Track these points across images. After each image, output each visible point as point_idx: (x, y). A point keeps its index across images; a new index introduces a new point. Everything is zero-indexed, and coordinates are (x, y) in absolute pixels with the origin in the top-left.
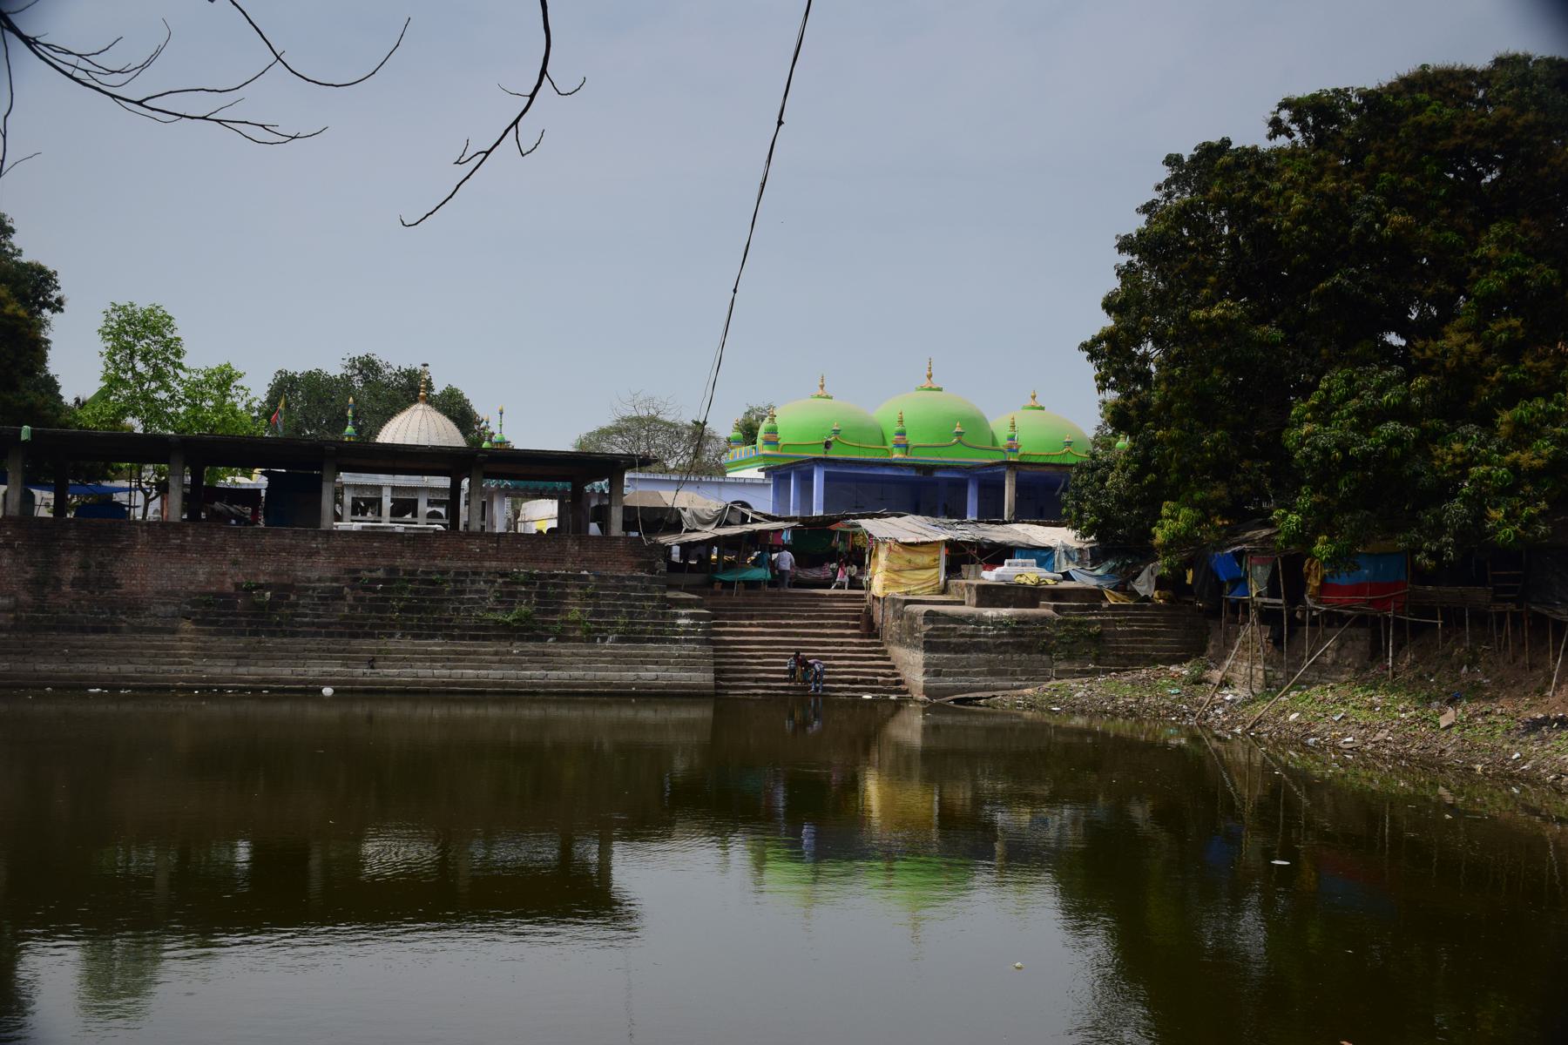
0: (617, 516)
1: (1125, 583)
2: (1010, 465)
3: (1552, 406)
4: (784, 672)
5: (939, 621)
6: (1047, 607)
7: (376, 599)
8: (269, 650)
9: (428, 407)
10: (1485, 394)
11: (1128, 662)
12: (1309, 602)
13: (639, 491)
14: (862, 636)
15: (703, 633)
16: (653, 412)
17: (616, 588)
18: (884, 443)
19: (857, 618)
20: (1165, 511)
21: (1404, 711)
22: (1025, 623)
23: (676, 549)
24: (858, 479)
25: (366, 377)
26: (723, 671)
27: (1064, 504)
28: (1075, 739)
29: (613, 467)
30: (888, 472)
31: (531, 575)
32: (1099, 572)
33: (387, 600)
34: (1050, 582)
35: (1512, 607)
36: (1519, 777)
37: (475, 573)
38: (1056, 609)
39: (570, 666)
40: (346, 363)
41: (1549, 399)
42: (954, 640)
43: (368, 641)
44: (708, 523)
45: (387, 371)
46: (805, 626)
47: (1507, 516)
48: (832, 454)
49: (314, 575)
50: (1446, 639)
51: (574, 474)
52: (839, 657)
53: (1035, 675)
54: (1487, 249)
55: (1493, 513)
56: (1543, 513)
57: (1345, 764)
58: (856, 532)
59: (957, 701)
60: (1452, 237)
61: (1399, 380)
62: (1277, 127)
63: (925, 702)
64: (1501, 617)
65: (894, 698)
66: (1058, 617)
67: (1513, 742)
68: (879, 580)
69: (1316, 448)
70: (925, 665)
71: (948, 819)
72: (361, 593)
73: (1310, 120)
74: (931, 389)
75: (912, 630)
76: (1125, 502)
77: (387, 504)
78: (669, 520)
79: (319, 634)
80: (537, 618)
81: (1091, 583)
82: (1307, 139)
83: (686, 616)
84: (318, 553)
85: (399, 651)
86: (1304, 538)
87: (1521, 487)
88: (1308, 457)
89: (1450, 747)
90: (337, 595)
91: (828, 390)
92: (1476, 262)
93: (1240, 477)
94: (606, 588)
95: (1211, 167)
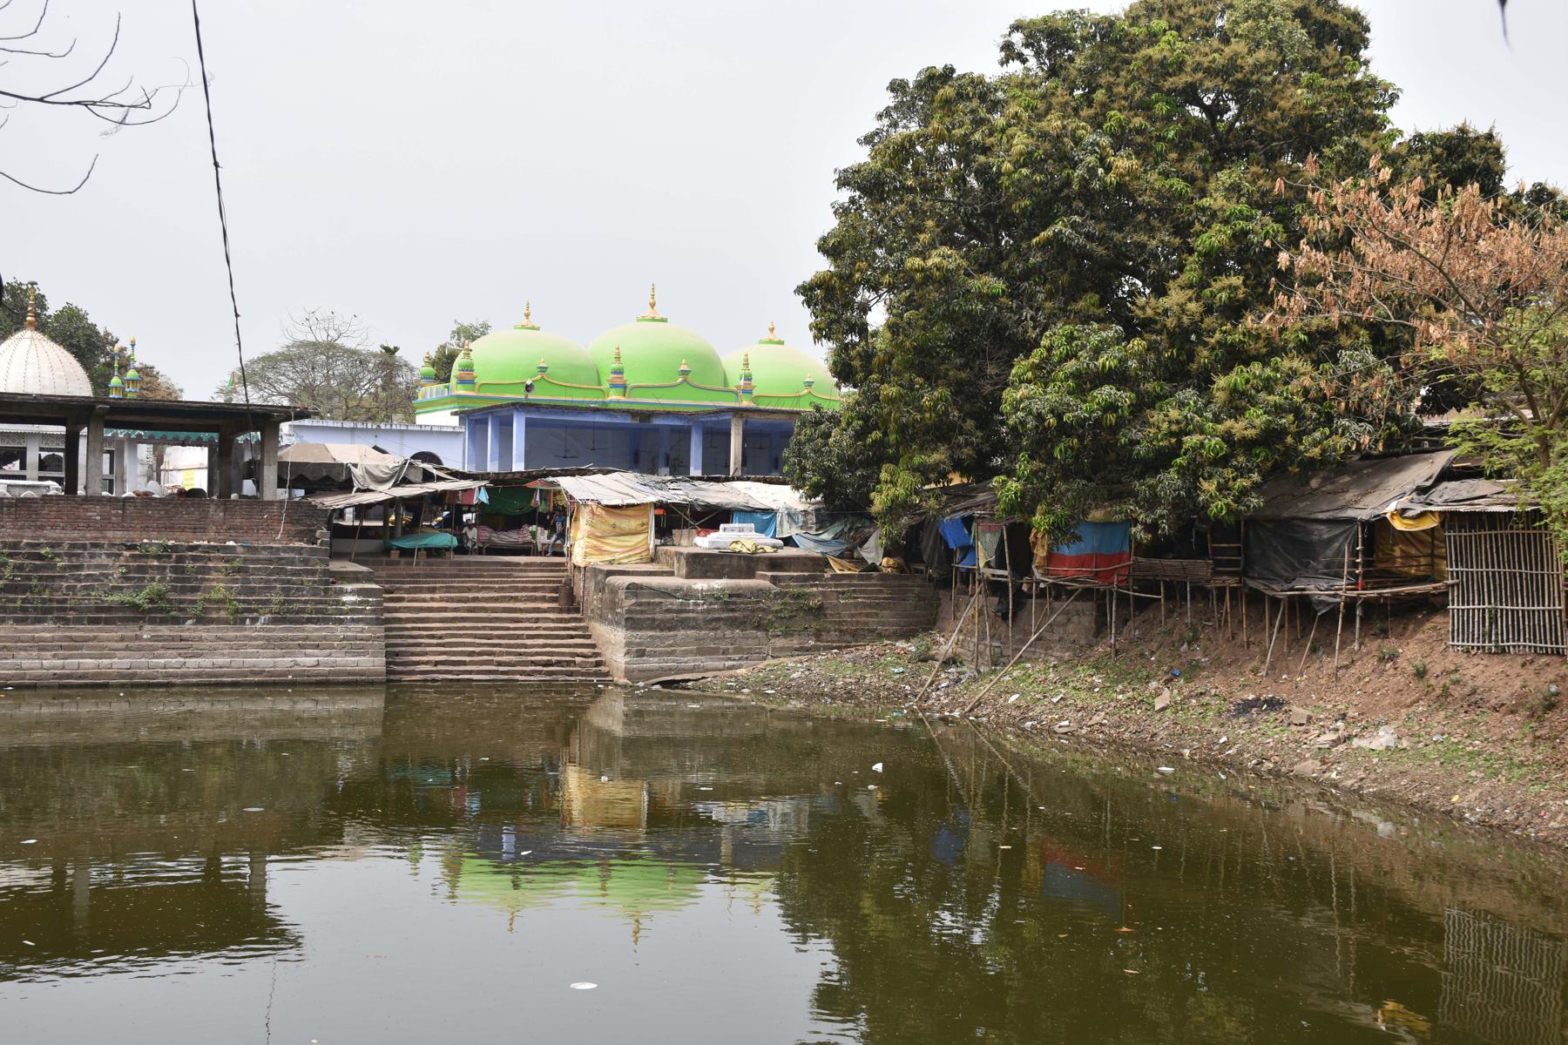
0: (270, 474)
1: (851, 550)
3: (1268, 371)
5: (643, 596)
6: (764, 577)
9: (38, 335)
10: (1204, 355)
11: (853, 636)
13: (295, 443)
14: (560, 611)
15: (373, 612)
16: (333, 334)
17: (270, 561)
19: (555, 590)
20: (884, 476)
21: (1122, 692)
22: (738, 596)
26: (397, 654)
28: (793, 725)
29: (266, 420)
30: (599, 419)
31: (166, 548)
32: (825, 536)
34: (769, 549)
35: (1232, 582)
36: (1224, 763)
37: (95, 545)
38: (774, 580)
42: (659, 616)
46: (496, 600)
47: (1220, 488)
48: (533, 397)
50: (1170, 613)
53: (747, 654)
55: (1205, 485)
56: (1256, 486)
57: (1062, 749)
58: (554, 493)
59: (664, 684)
60: (1179, 184)
61: (1118, 341)
63: (625, 686)
64: (1221, 591)
65: (595, 681)
67: (1222, 725)
68: (582, 546)
69: (1030, 413)
70: (628, 644)
71: (659, 817)
73: (1044, 45)
74: (653, 319)
75: (613, 605)
76: (849, 463)
78: (336, 479)
80: (172, 596)
83: (353, 592)
86: (1024, 504)
87: (1234, 456)
88: (1023, 423)
89: (1161, 729)
93: (961, 439)
94: (257, 561)
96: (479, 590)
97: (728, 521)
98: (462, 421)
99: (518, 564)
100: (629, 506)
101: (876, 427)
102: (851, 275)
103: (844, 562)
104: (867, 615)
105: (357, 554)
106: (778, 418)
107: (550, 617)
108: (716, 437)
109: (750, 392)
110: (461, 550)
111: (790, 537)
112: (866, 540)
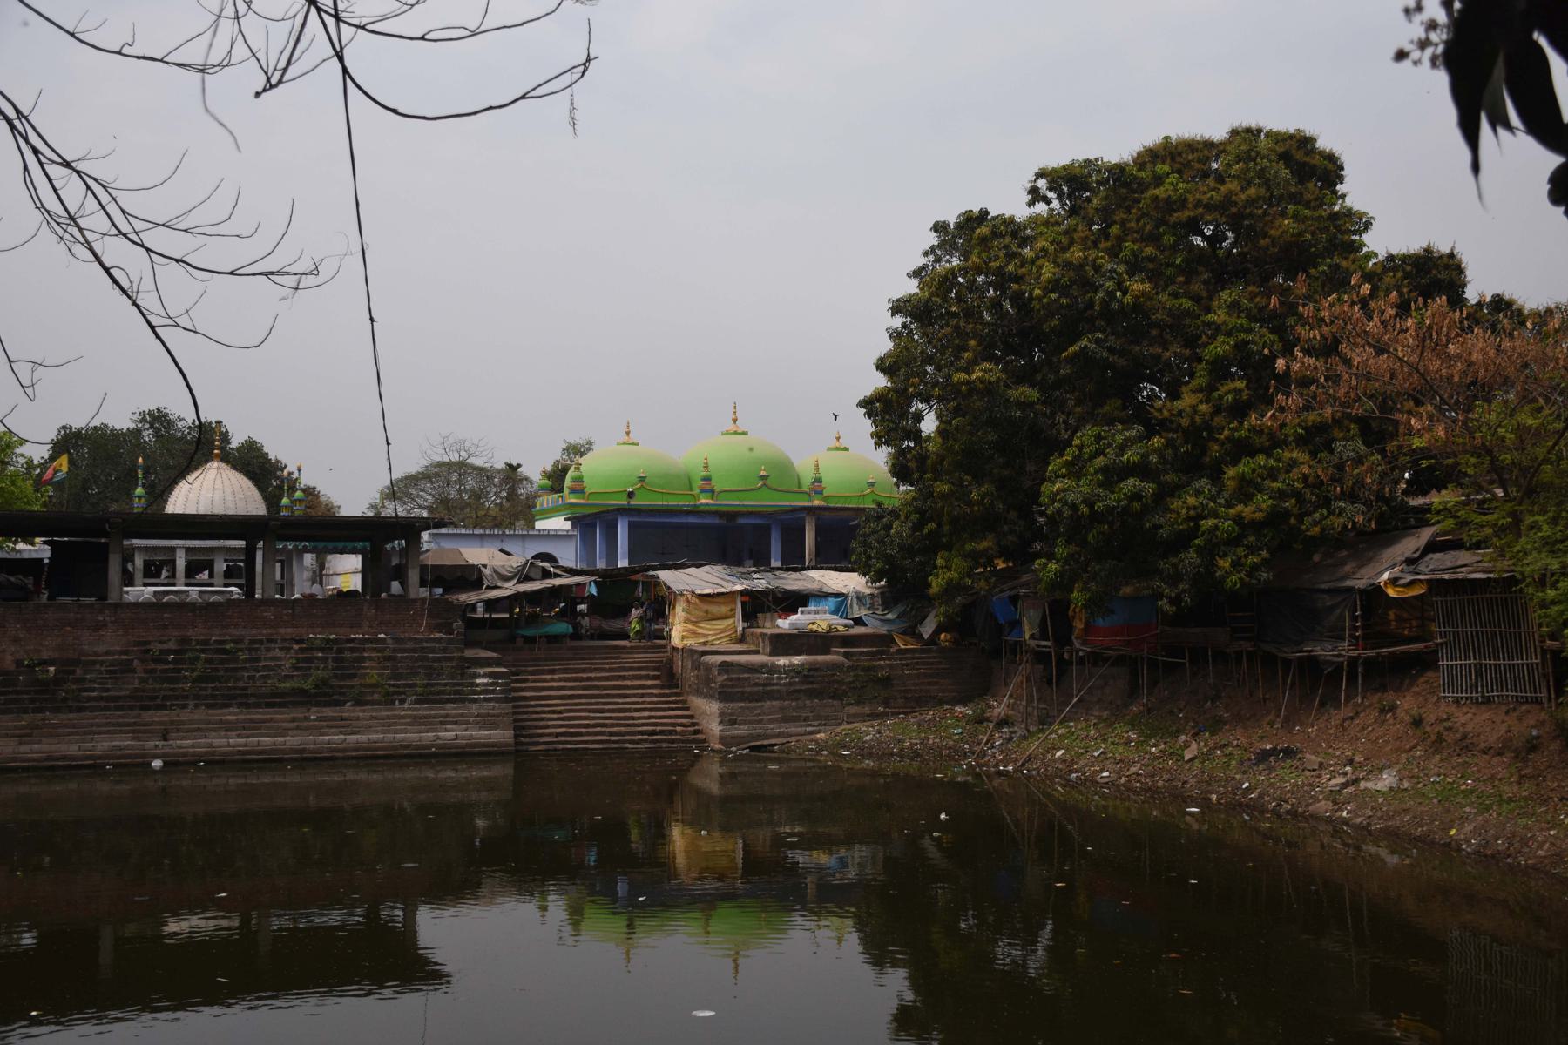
0: (413, 576)
1: (914, 627)
2: (811, 510)
3: (1272, 462)
6: (837, 653)
7: (166, 671)
8: (54, 726)
9: (223, 465)
11: (915, 702)
12: (1077, 645)
14: (662, 687)
15: (502, 692)
16: (464, 454)
17: (414, 650)
20: (940, 562)
23: (480, 607)
25: (157, 431)
26: (524, 728)
27: (853, 551)
29: (409, 529)
30: (691, 520)
32: (889, 616)
33: (179, 671)
34: (841, 629)
36: (1247, 805)
37: (269, 641)
38: (846, 655)
39: (368, 729)
40: (136, 417)
41: (1269, 456)
43: (159, 713)
44: (507, 579)
45: (180, 425)
46: (607, 679)
49: (102, 648)
51: (374, 536)
53: (826, 721)
54: (1219, 316)
55: (1221, 563)
56: (1265, 562)
58: (657, 583)
59: (752, 749)
60: (1187, 303)
61: (1140, 439)
62: (1035, 195)
65: (691, 746)
66: (848, 663)
68: (679, 631)
69: (1066, 503)
70: (721, 715)
71: (754, 865)
72: (153, 666)
74: (736, 433)
75: (708, 681)
76: (907, 550)
77: (181, 563)
78: (470, 577)
79: (106, 708)
80: (334, 682)
82: (1062, 205)
83: (485, 676)
84: (105, 626)
85: (191, 722)
86: (1063, 584)
88: (1059, 512)
90: (127, 668)
91: (634, 437)
92: (1209, 324)
93: (1006, 528)
95: (971, 233)
96: (592, 670)
98: (574, 526)
100: (719, 594)
101: (931, 519)
102: (906, 389)
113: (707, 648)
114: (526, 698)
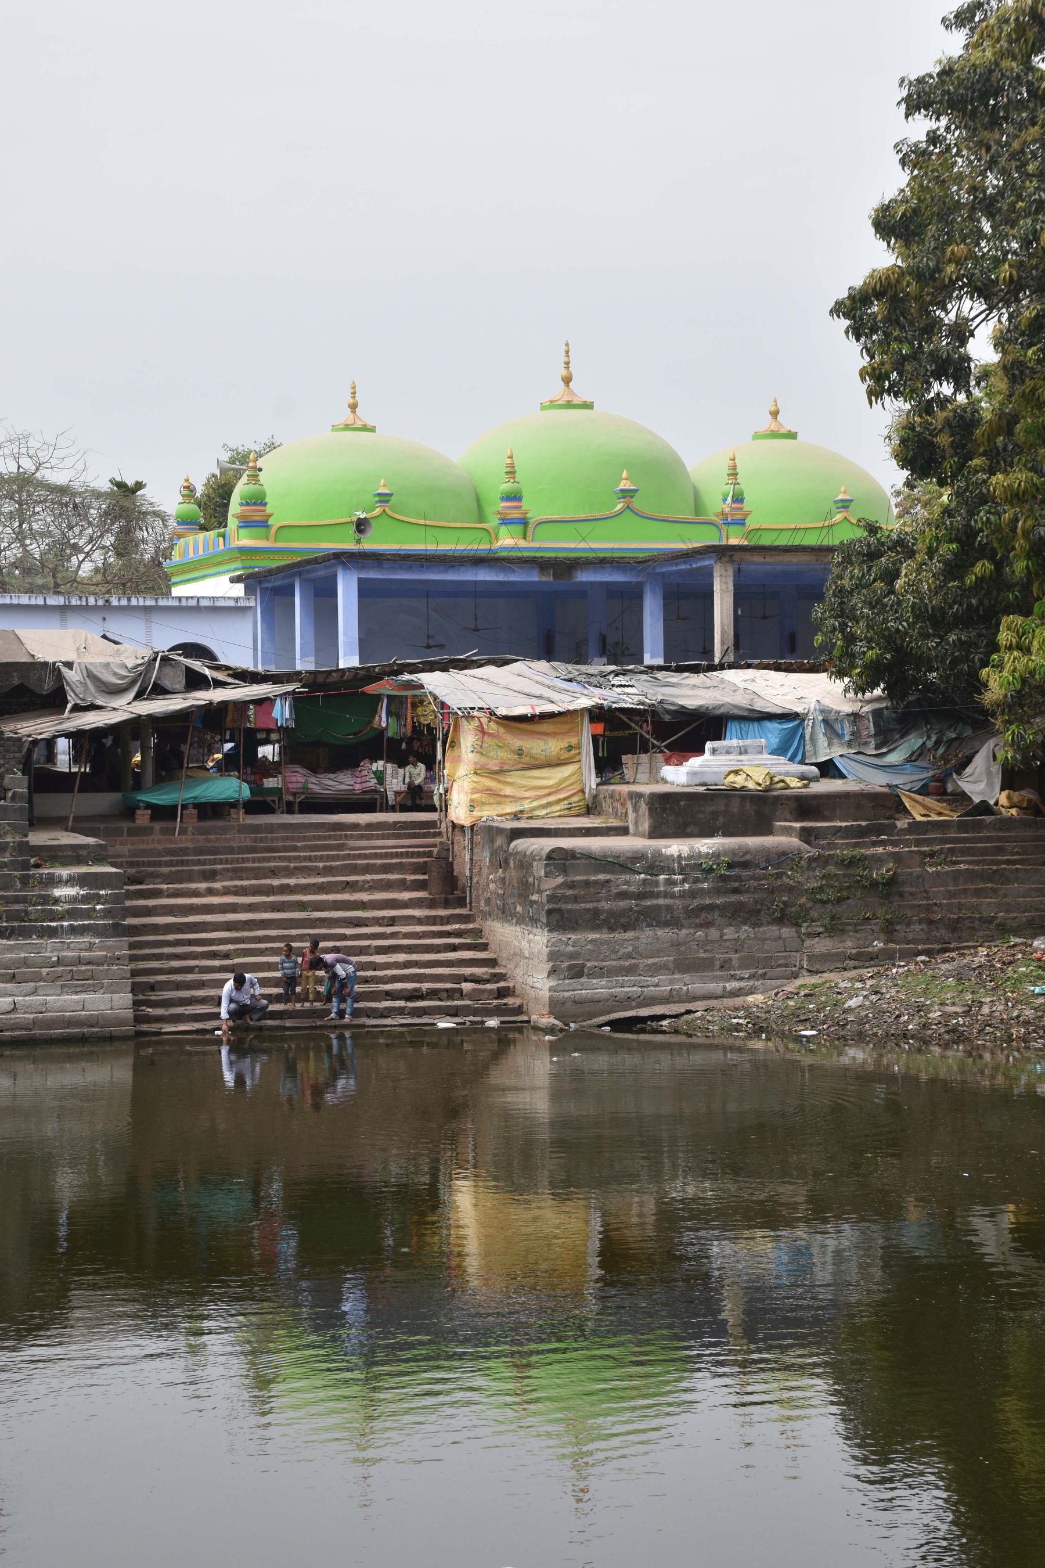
1: (942, 780)
2: (723, 552)
4: (276, 982)
6: (787, 831)
11: (951, 933)
14: (432, 904)
15: (107, 913)
16: (28, 465)
18: (481, 517)
20: (1004, 637)
22: (744, 865)
24: (428, 590)
26: (152, 987)
27: (817, 628)
30: (484, 575)
34: (794, 783)
38: (806, 835)
42: (606, 905)
44: (117, 691)
48: (370, 543)
52: (386, 948)
53: (765, 967)
59: (617, 1025)
66: (809, 851)
68: (464, 792)
70: (552, 956)
74: (569, 405)
75: (525, 889)
76: (935, 620)
81: (876, 781)
83: (71, 881)
91: (365, 415)
96: (290, 873)
97: (718, 736)
98: (248, 590)
99: (355, 826)
100: (545, 717)
101: (986, 552)
102: (938, 269)
103: (929, 801)
104: (978, 893)
105: (76, 819)
106: (794, 558)
107: (415, 913)
108: (688, 601)
109: (742, 523)
110: (254, 807)
111: (831, 761)
112: (968, 761)
113: (522, 824)
114: (156, 929)
